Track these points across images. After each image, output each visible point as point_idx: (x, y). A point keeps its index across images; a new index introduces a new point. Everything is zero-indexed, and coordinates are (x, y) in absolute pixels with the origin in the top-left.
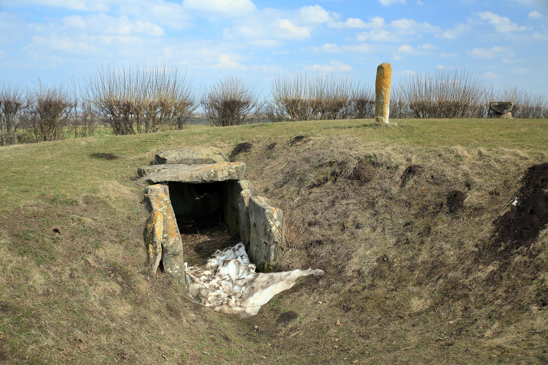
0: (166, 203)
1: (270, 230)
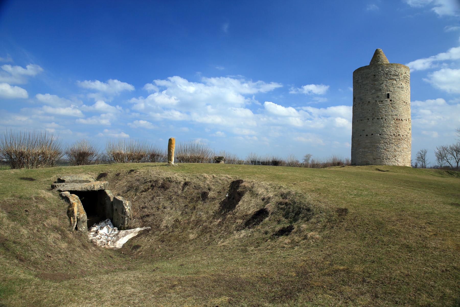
0: (77, 198)
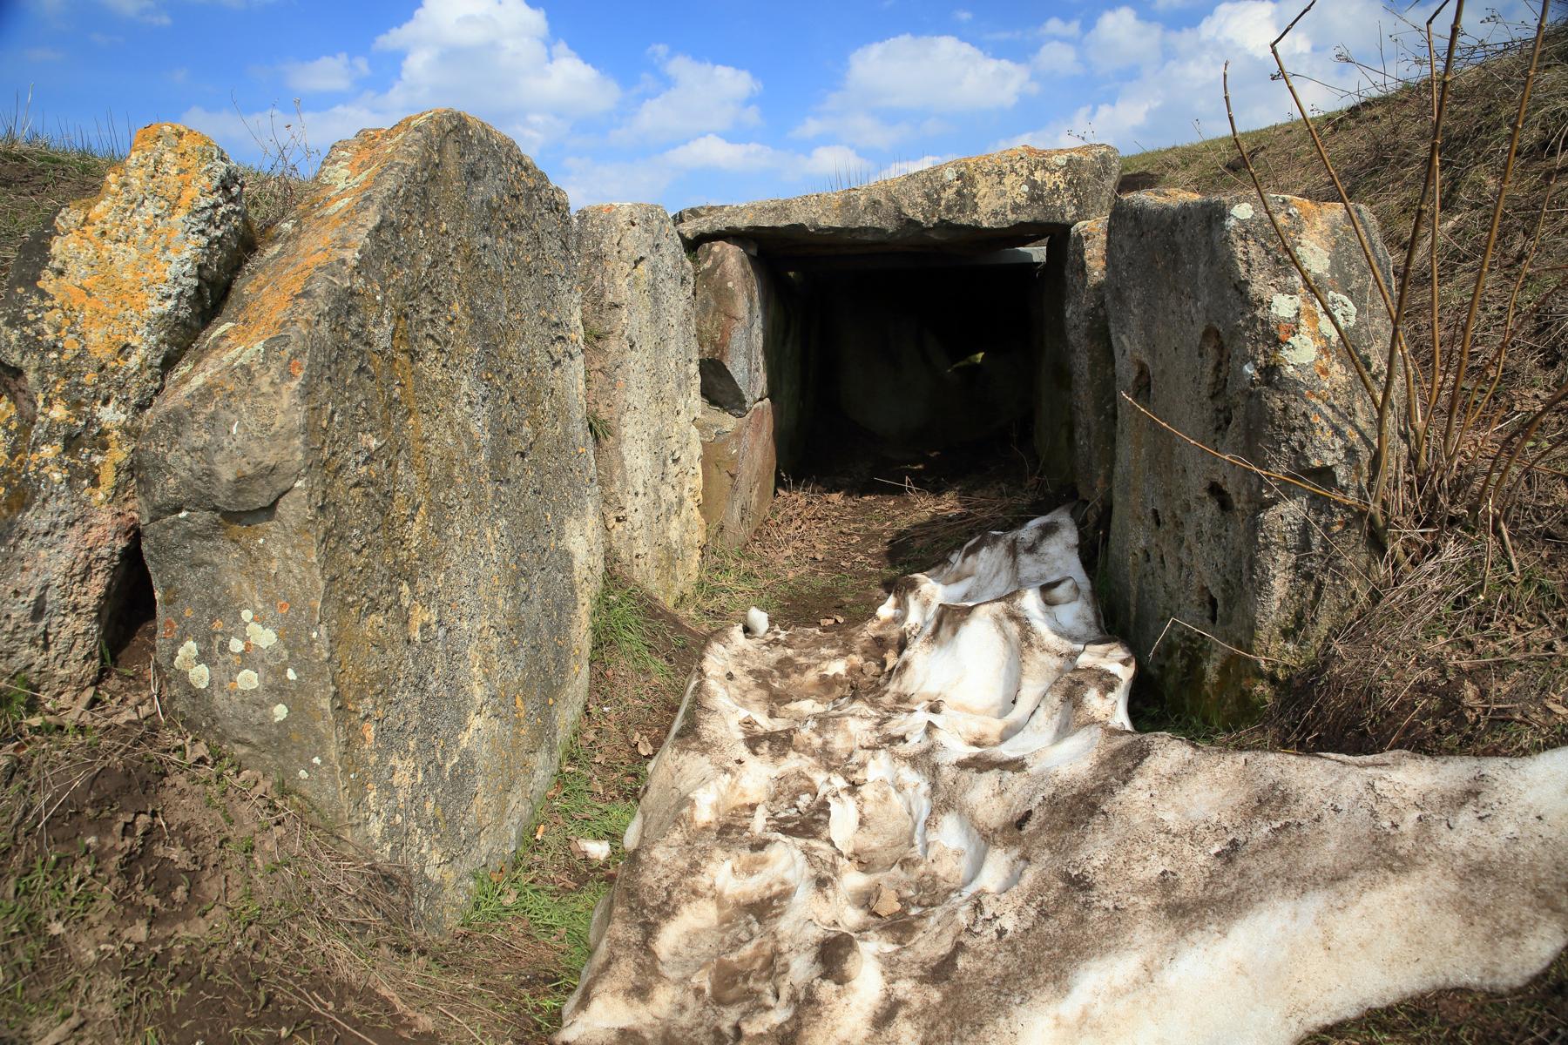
1: (1270, 372)
